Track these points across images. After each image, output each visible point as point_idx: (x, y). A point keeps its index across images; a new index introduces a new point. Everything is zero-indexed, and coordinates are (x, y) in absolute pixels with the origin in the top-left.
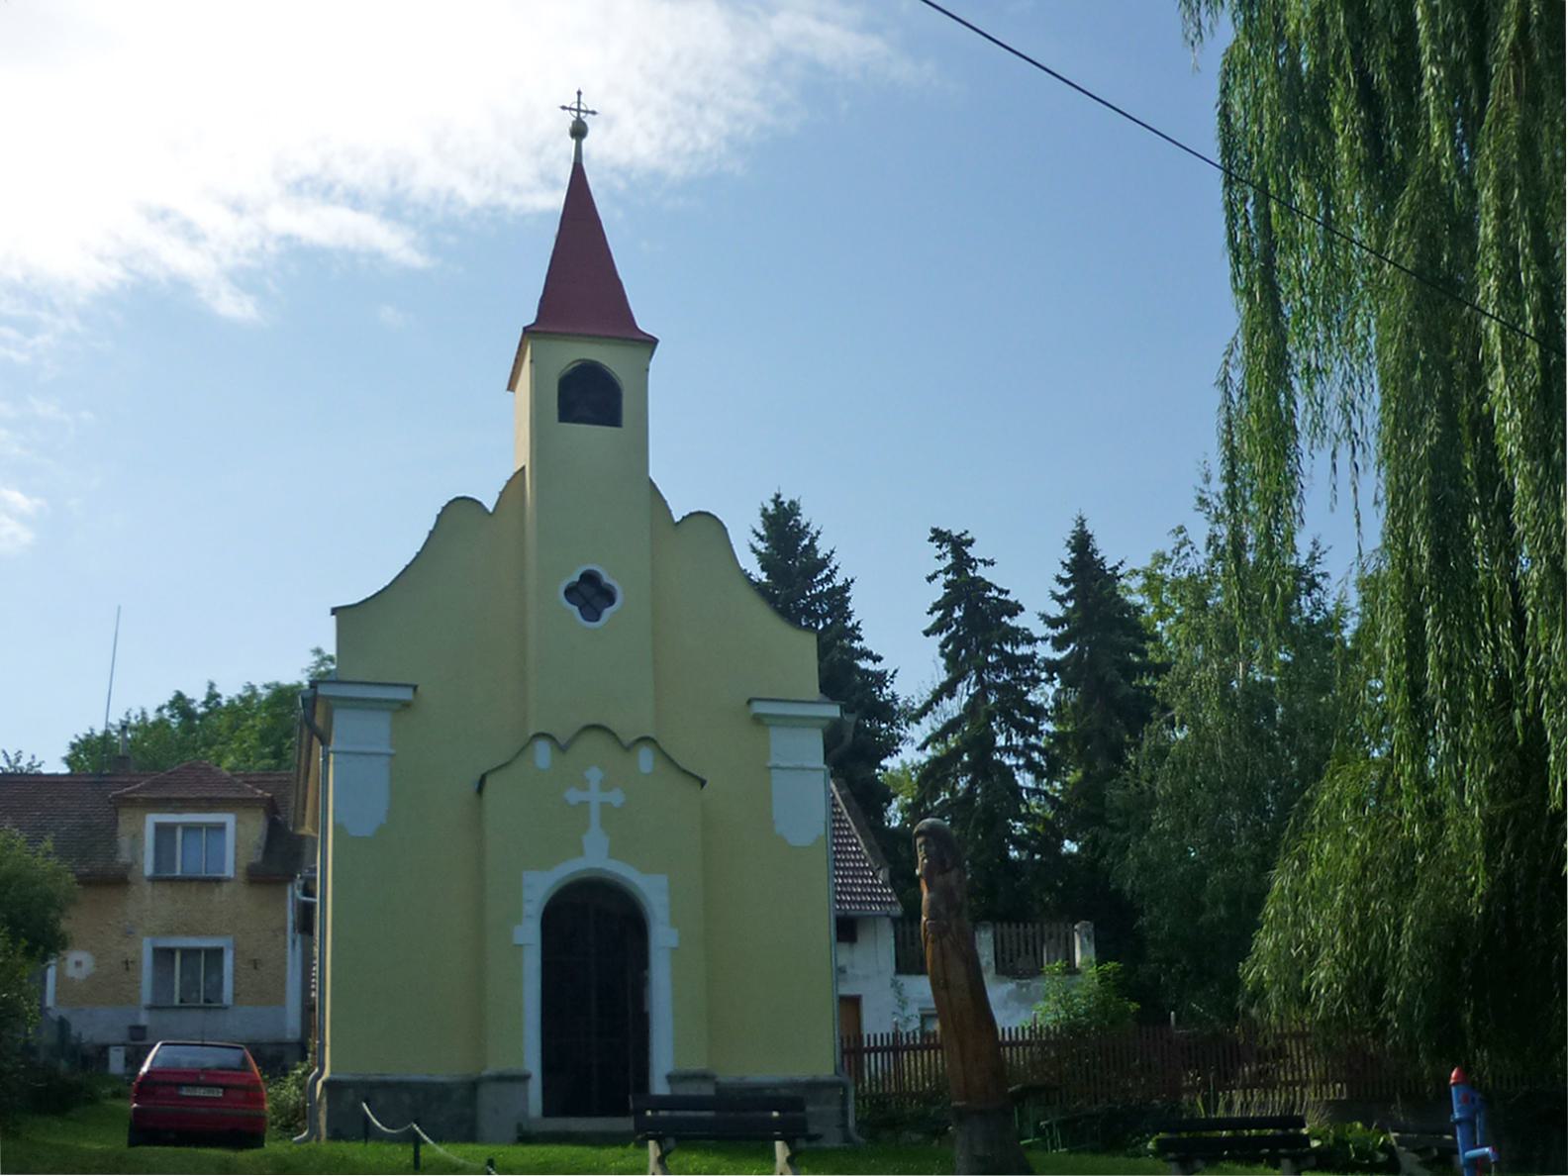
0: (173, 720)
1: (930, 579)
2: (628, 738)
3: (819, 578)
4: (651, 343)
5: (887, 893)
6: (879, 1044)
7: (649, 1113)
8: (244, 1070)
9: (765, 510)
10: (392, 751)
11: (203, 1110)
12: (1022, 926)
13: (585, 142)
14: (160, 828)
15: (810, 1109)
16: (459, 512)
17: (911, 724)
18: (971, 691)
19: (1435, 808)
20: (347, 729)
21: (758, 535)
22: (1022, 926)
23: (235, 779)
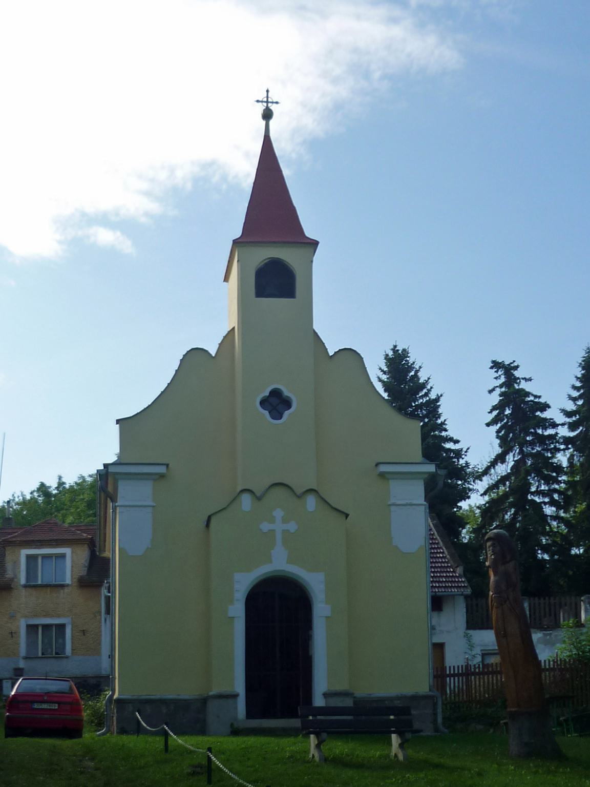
0: (40, 498)
1: (490, 392)
2: (299, 491)
3: (420, 395)
4: (314, 244)
5: (462, 581)
6: (460, 672)
7: (311, 718)
8: (72, 694)
9: (387, 355)
10: (155, 504)
11: (46, 716)
12: (547, 598)
13: (271, 122)
14: (29, 558)
15: (413, 712)
16: (195, 355)
17: (476, 481)
18: (516, 459)
19: (106, 743)
20: (127, 493)
21: (382, 371)
22: (547, 598)
23: (71, 528)
